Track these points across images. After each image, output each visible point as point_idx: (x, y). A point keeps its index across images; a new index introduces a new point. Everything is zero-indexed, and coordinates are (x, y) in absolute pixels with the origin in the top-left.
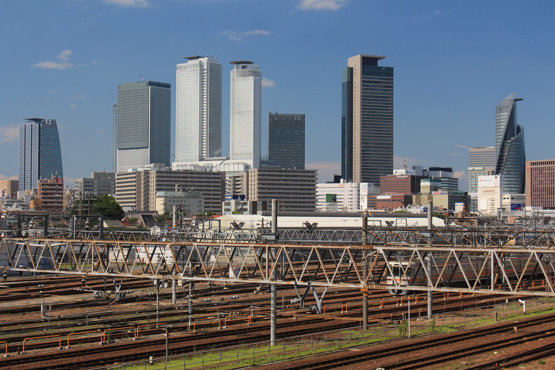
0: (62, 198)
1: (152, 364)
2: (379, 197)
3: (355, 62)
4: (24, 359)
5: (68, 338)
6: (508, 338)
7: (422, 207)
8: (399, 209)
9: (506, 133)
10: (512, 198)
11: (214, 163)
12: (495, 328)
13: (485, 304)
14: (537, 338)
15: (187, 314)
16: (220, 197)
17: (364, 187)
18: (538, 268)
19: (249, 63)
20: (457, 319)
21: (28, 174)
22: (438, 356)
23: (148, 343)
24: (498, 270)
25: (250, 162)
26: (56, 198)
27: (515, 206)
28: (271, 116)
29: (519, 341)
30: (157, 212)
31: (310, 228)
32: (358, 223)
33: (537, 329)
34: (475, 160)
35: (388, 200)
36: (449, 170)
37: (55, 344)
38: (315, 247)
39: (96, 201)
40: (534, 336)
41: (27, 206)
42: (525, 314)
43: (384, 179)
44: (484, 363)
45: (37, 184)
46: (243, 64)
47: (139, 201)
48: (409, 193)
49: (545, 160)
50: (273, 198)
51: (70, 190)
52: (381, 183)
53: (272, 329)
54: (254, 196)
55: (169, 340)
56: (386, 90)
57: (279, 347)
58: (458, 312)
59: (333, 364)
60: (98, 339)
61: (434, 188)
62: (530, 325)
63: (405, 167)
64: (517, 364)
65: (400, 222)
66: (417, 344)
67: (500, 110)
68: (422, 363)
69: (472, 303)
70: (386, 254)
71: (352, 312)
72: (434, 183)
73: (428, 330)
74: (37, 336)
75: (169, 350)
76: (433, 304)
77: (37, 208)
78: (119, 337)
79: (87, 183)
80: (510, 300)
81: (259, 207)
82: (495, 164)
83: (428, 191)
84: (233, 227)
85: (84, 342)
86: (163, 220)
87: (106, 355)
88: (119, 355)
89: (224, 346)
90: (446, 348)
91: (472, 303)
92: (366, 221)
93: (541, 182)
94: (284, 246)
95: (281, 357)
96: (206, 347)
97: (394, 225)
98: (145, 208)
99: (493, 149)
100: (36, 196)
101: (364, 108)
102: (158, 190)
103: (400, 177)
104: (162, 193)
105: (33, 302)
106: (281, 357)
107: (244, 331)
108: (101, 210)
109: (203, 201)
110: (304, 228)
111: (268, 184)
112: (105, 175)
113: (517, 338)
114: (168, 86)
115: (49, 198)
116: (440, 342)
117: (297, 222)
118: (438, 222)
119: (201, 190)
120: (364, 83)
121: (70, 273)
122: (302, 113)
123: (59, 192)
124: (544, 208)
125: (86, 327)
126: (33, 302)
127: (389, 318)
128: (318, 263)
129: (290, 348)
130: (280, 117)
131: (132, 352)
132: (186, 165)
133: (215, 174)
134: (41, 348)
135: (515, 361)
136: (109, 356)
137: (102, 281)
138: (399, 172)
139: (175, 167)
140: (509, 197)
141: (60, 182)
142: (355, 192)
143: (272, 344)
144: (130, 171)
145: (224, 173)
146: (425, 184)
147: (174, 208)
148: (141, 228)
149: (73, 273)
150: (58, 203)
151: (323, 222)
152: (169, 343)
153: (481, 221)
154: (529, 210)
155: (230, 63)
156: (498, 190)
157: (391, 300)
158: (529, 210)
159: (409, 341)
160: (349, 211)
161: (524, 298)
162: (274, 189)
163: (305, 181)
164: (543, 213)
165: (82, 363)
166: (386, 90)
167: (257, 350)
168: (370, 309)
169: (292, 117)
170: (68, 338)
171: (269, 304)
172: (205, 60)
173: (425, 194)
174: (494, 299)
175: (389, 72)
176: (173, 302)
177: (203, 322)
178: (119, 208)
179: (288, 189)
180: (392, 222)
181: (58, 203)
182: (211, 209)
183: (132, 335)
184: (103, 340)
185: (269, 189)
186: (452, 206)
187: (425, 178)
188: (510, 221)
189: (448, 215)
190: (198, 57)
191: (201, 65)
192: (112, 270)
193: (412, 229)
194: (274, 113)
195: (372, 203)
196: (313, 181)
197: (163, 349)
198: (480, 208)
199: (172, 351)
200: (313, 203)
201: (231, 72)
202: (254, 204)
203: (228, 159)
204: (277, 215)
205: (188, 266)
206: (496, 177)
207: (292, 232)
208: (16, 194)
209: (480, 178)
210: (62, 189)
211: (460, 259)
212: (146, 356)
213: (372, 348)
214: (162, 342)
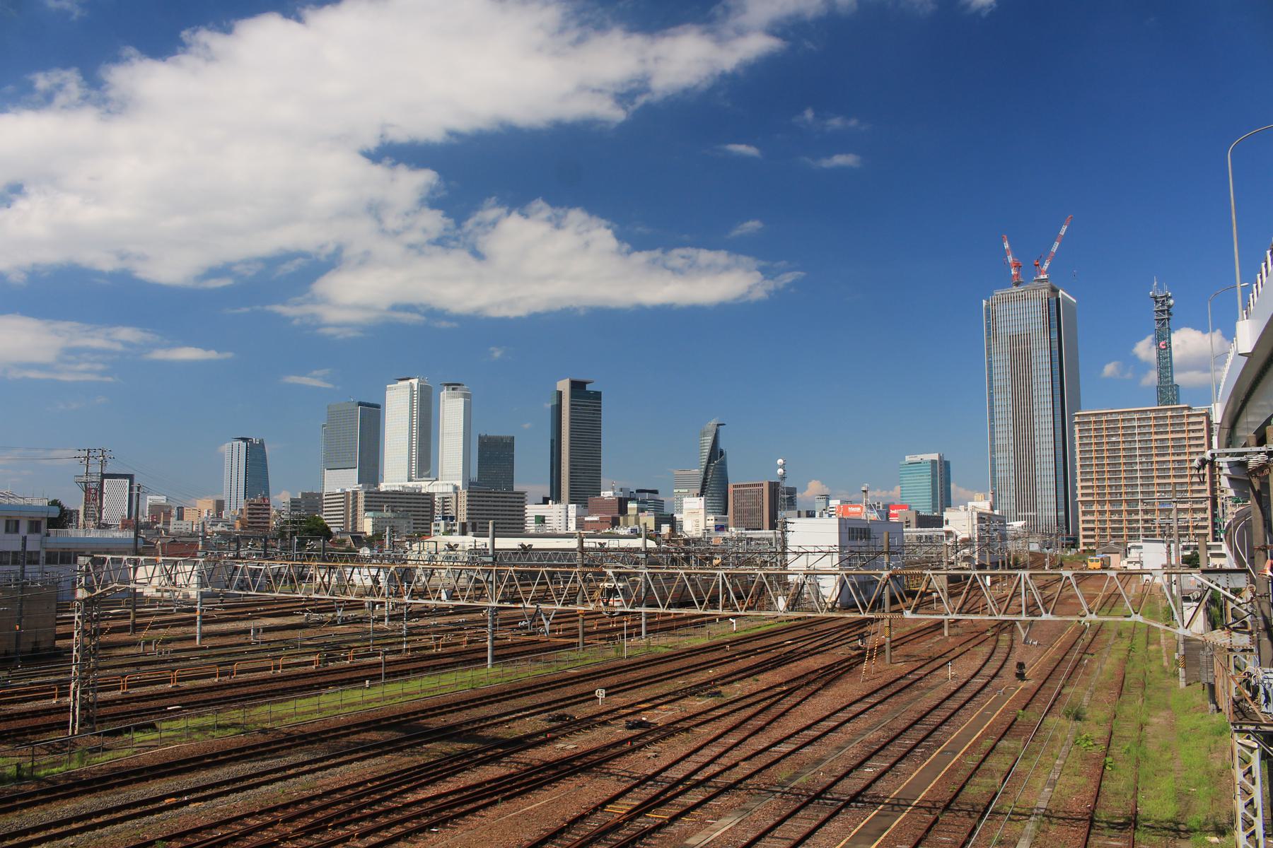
0: (269, 518)
1: (369, 688)
2: (586, 519)
3: (564, 386)
4: (235, 684)
5: (281, 662)
6: (721, 656)
7: (629, 528)
8: (607, 531)
9: (710, 457)
10: (716, 520)
11: (423, 484)
12: (708, 647)
13: (696, 623)
14: (749, 656)
15: (402, 636)
16: (428, 518)
17: (572, 508)
18: (685, 593)
19: (459, 385)
20: (671, 639)
21: (234, 494)
22: (655, 676)
23: (363, 667)
24: (726, 591)
25: (459, 483)
26: (263, 518)
28: (480, 437)
29: (732, 659)
30: (365, 533)
31: (526, 549)
32: (573, 544)
33: (748, 647)
34: (682, 482)
35: (597, 521)
36: (656, 492)
37: (268, 669)
38: (544, 569)
39: (304, 521)
40: (747, 654)
41: (233, 526)
42: (735, 632)
43: (592, 500)
44: (700, 682)
45: (242, 504)
46: (454, 386)
47: (347, 522)
48: (616, 515)
49: (741, 484)
50: (491, 519)
51: (277, 510)
52: (589, 505)
53: (489, 651)
54: (463, 517)
55: (385, 662)
56: (594, 414)
57: (496, 669)
58: (673, 632)
59: (513, 695)
60: (311, 663)
61: (641, 510)
62: (741, 643)
63: (613, 489)
64: (732, 682)
65: (612, 544)
66: (633, 665)
67: (704, 434)
68: (639, 683)
69: (683, 622)
70: (615, 575)
71: (567, 633)
73: (642, 651)
74: (248, 659)
75: (386, 674)
76: (647, 624)
77: (243, 528)
78: (332, 661)
79: (295, 504)
80: (720, 619)
81: (469, 528)
82: (700, 486)
83: (635, 512)
84: (447, 548)
85: (297, 666)
86: (370, 542)
87: (321, 680)
88: (334, 679)
89: (441, 669)
90: (663, 668)
91: (683, 622)
92: (582, 542)
93: (743, 504)
94: (512, 568)
95: (500, 680)
96: (422, 670)
97: (606, 546)
98: (353, 529)
99: (698, 472)
100: (242, 517)
101: (572, 430)
102: (366, 510)
104: (371, 514)
105: (242, 625)
106: (500, 680)
107: (461, 653)
108: (310, 531)
109: (412, 522)
110: (519, 550)
111: (478, 505)
112: (312, 494)
113: (730, 657)
114: (378, 406)
115: (256, 518)
116: (523, 692)
117: (512, 543)
118: (651, 544)
119: (410, 511)
120: (573, 406)
121: (291, 596)
122: (511, 435)
123: (266, 512)
124: (746, 529)
125: (298, 651)
126: (242, 625)
127: (604, 639)
128: (546, 583)
129: (508, 670)
130: (490, 438)
131: (348, 675)
132: (395, 486)
133: (424, 494)
134: (253, 672)
135: (730, 679)
136: (325, 680)
137: (313, 603)
138: (607, 494)
139: (383, 487)
140: (713, 518)
141: (267, 501)
142: (563, 514)
143: (489, 666)
144: (338, 491)
145: (434, 494)
146: (632, 506)
147: (388, 528)
148: (349, 549)
149: (294, 596)
150: (265, 523)
151: (538, 543)
152: (385, 666)
153: (687, 542)
154: (733, 531)
156: (702, 512)
157: (604, 621)
158: (733, 531)
159: (625, 662)
160: (558, 532)
161: (733, 617)
162: (483, 510)
163: (514, 502)
164: (746, 534)
165: (296, 687)
166: (594, 414)
167: (475, 673)
168: (585, 629)
169: (502, 439)
170: (281, 662)
171: (486, 626)
172: (415, 382)
173: (632, 515)
174: (706, 618)
175: (597, 396)
176: (385, 625)
177: (417, 645)
178: (328, 529)
179: (498, 510)
180: (605, 543)
181: (265, 523)
182: (419, 530)
183: (346, 658)
184: (124, 688)
185: (478, 510)
186: (658, 527)
187: (632, 499)
188: (714, 541)
189: (654, 536)
190: (408, 379)
191: (411, 386)
192: (334, 593)
193: (630, 550)
194: (483, 434)
195: (580, 524)
196: (523, 502)
197: (379, 672)
198: (685, 529)
199: (388, 675)
200: (522, 524)
201: (442, 393)
202: (464, 525)
203: (437, 480)
204: (494, 537)
205: (573, 585)
207: (507, 554)
208: (221, 514)
209: (686, 500)
210: (269, 509)
211: (652, 580)
212: (362, 679)
213: (589, 669)
214: (379, 665)
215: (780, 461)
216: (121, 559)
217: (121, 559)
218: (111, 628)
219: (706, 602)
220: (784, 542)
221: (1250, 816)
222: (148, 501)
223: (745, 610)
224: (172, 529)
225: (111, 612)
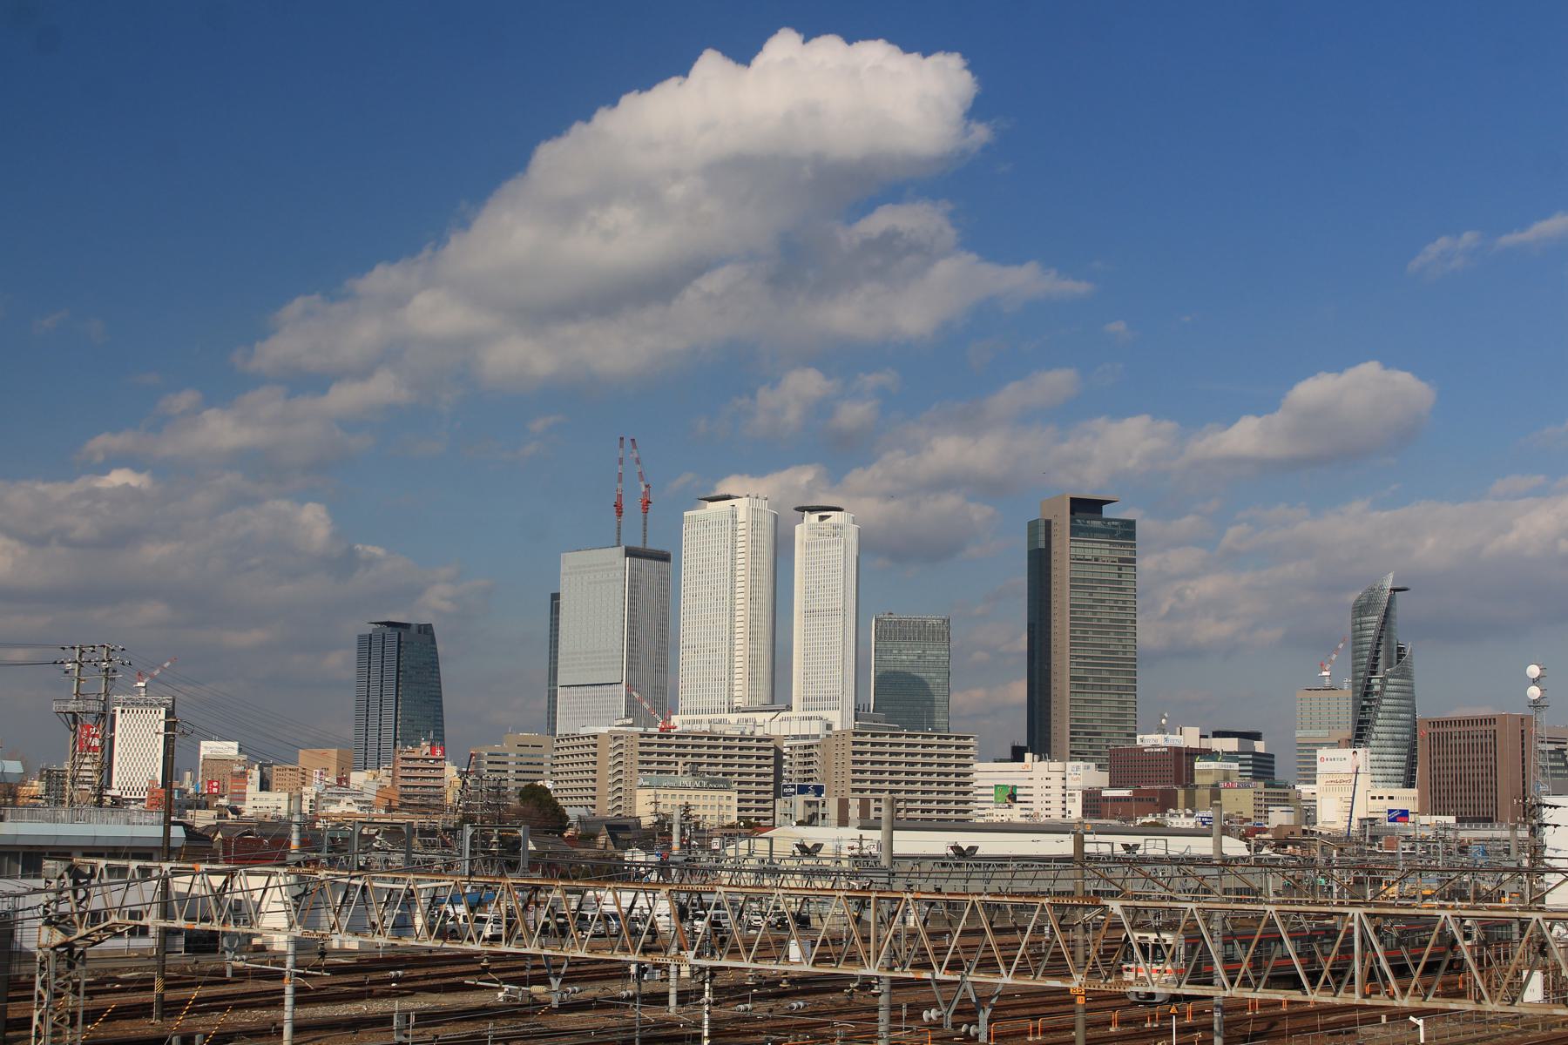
8: (1149, 819)
35: (1126, 799)
65: (1152, 846)
70: (1127, 913)
72: (1224, 764)
92: (1080, 843)
97: (1139, 852)
103: (1152, 750)
105: (376, 1007)
114: (664, 557)
126: (376, 1007)
132: (700, 722)
139: (678, 722)
161: (1419, 1013)
175: (1127, 530)
180: (1137, 846)
203: (789, 708)
206: (1355, 752)
215: (1534, 671)
217: (126, 869)
218: (178, 1013)
219: (1326, 973)
220: (1537, 851)
223: (814, 964)
224: (248, 810)
225: (122, 976)
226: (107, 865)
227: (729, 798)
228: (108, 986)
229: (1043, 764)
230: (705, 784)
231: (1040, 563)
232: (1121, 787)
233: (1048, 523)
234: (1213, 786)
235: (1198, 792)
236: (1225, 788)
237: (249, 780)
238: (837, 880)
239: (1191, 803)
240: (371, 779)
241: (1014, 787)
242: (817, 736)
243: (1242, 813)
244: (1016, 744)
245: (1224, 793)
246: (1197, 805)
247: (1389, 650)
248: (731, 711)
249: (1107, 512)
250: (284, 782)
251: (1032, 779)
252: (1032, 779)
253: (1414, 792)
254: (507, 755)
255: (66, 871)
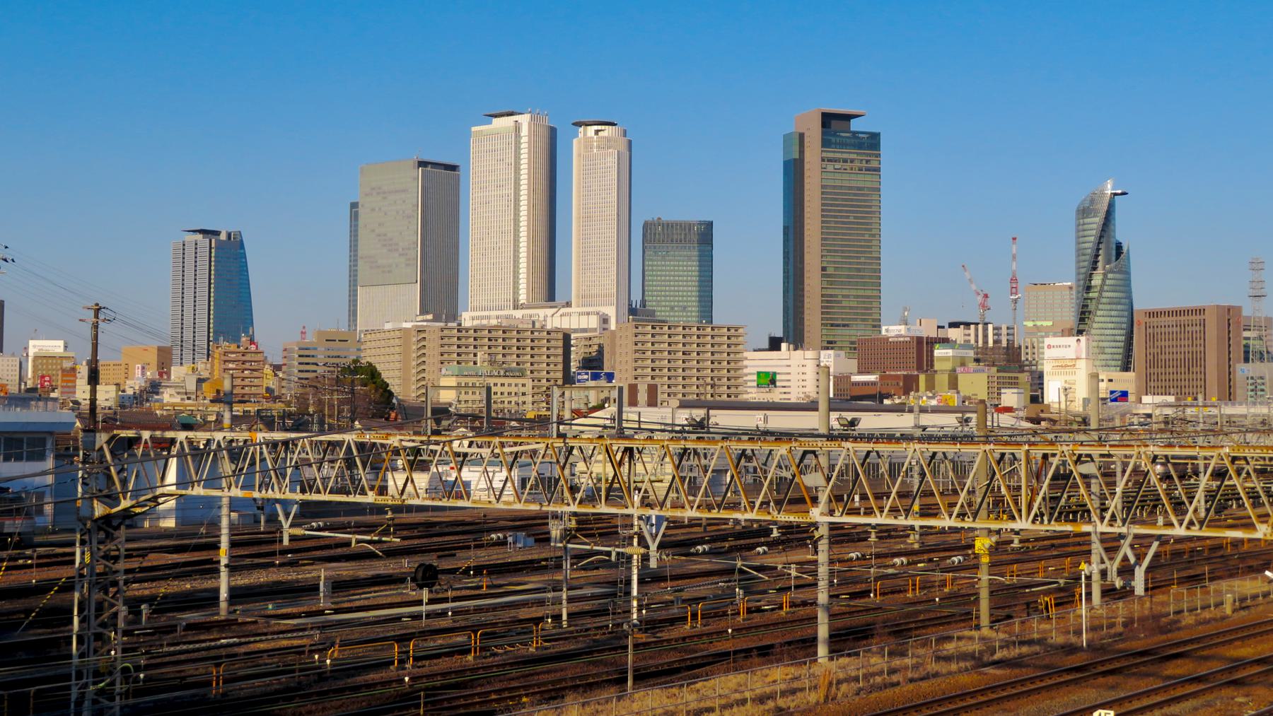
25: (611, 311)
27: (1117, 395)
103: (896, 339)
114: (453, 168)
132: (488, 318)
155: (574, 124)
162: (850, 251)
172: (524, 120)
175: (872, 142)
203: (568, 304)
206: (1078, 340)
216: (137, 440)
221: (1132, 560)
222: (32, 352)
226: (187, 438)
227: (524, 385)
228: (21, 562)
229: (799, 352)
230: (502, 373)
231: (794, 171)
232: (868, 373)
233: (802, 136)
234: (950, 371)
235: (937, 377)
236: (962, 373)
237: (78, 375)
238: (142, 474)
239: (931, 386)
240: (190, 372)
241: (775, 374)
242: (595, 330)
243: (976, 395)
244: (772, 335)
245: (960, 377)
246: (936, 389)
247: (1108, 248)
248: (516, 307)
249: (855, 125)
250: (108, 372)
251: (789, 366)
252: (789, 366)
253: (1130, 375)
254: (315, 349)
255: (106, 443)
